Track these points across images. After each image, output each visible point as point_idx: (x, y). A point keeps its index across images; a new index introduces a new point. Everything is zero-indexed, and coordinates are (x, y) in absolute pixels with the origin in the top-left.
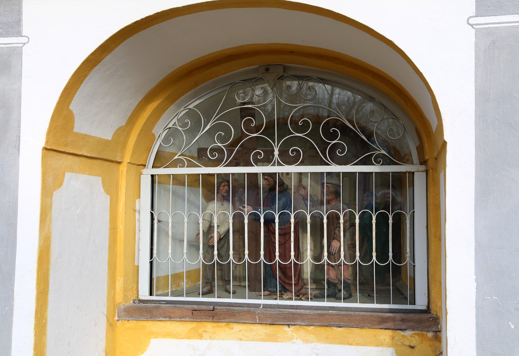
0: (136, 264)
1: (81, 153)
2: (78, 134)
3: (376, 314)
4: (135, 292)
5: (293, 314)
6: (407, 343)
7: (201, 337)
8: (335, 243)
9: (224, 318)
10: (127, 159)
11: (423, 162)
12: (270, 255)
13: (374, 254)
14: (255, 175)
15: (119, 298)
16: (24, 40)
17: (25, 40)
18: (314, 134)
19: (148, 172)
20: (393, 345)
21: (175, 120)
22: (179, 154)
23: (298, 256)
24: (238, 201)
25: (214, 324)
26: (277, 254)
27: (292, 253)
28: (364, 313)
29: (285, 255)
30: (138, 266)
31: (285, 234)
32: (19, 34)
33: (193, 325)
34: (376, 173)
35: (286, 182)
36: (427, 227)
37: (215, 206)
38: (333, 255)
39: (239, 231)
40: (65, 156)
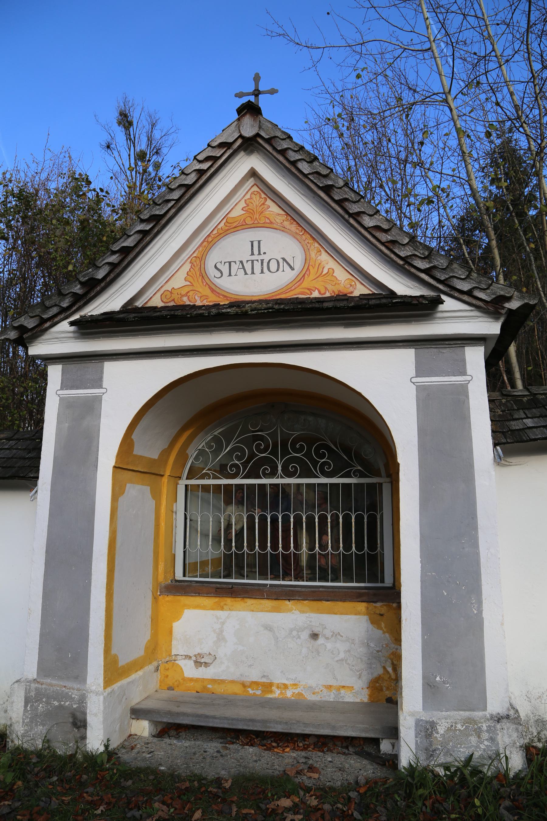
0: (173, 552)
1: (137, 469)
2: (136, 456)
3: (355, 590)
4: (172, 574)
5: (292, 591)
6: (378, 612)
7: (222, 609)
8: (324, 537)
9: (240, 595)
10: (168, 473)
11: (389, 475)
12: (275, 546)
13: (354, 545)
14: (264, 485)
15: (161, 578)
16: (103, 391)
17: (104, 391)
18: (308, 455)
19: (183, 482)
20: (368, 614)
21: (204, 443)
22: (207, 469)
23: (297, 546)
24: (251, 506)
25: (233, 599)
26: (280, 546)
27: (292, 545)
28: (346, 590)
29: (286, 546)
30: (175, 555)
31: (286, 530)
32: (101, 387)
33: (217, 599)
34: (354, 484)
35: (287, 490)
36: (393, 524)
37: (232, 510)
38: (323, 547)
39: (251, 528)
40: (126, 471)
